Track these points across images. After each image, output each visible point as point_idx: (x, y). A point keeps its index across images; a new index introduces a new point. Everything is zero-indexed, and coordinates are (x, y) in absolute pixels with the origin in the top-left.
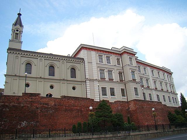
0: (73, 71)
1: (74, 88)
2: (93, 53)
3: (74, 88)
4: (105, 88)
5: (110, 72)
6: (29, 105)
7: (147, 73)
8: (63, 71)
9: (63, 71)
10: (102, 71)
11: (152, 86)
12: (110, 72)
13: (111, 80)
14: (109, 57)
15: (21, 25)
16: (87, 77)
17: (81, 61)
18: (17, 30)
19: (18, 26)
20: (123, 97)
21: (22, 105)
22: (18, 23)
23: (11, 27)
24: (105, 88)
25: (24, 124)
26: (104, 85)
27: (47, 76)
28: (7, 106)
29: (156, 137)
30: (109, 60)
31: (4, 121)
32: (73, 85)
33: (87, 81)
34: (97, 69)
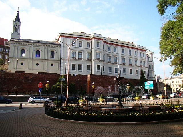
0: (53, 54)
1: (52, 65)
2: (68, 39)
3: (37, 64)
4: (75, 65)
5: (80, 54)
6: (18, 78)
7: (145, 56)
8: (45, 53)
9: (45, 53)
10: (74, 53)
11: (139, 64)
12: (80, 54)
13: (80, 59)
14: (116, 48)
15: (19, 21)
16: (62, 57)
17: (59, 46)
18: (16, 25)
19: (17, 22)
20: (98, 71)
21: (14, 78)
22: (18, 19)
23: (12, 23)
24: (75, 65)
25: (15, 88)
26: (74, 62)
27: (49, 58)
28: (7, 78)
29: (120, 93)
30: (124, 51)
31: (5, 86)
32: (51, 63)
33: (61, 60)
34: (121, 58)
